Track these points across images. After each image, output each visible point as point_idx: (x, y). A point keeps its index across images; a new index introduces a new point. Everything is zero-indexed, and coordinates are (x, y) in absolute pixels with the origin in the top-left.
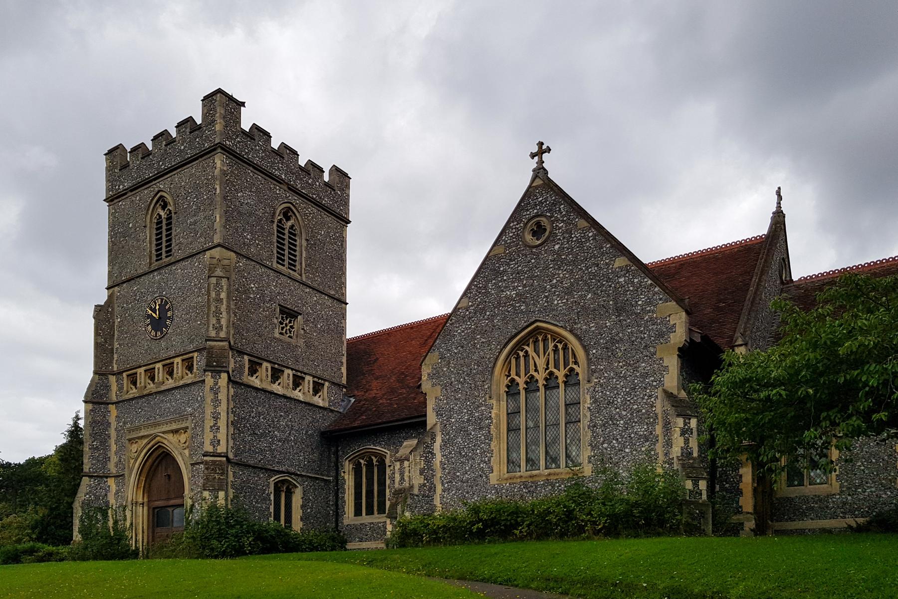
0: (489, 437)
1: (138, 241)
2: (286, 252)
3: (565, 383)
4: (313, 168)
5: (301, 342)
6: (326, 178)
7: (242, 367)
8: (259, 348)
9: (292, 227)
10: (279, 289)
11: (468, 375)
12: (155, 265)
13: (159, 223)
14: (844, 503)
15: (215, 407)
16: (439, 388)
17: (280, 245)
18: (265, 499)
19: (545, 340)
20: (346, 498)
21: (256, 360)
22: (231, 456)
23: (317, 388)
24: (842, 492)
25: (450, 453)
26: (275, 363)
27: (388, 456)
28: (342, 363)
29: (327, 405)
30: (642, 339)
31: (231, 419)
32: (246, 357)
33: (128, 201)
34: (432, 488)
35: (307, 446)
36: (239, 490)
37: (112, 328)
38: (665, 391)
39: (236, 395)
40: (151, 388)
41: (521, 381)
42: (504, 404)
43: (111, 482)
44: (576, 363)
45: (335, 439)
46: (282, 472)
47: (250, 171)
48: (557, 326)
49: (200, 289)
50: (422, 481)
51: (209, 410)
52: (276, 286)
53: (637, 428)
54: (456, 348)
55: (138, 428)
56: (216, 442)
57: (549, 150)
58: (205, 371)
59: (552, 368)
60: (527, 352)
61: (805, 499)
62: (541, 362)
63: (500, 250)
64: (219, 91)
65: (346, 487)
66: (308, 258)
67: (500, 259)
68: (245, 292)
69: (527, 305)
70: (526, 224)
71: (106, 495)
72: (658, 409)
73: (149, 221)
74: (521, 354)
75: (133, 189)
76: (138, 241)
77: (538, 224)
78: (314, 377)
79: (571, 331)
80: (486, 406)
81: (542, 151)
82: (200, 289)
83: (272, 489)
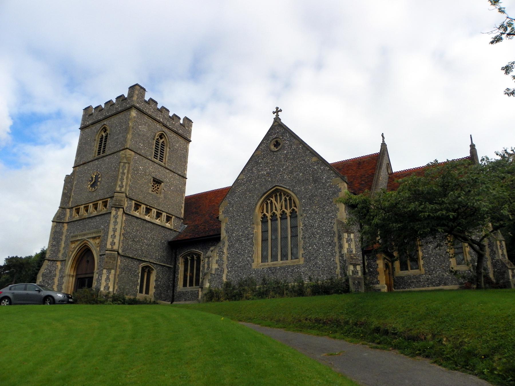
0: (252, 244)
1: (91, 146)
2: (159, 153)
3: (290, 216)
4: (176, 117)
5: (162, 196)
6: (181, 121)
7: (131, 206)
8: (140, 198)
9: (163, 142)
10: (154, 170)
11: (242, 212)
12: (97, 157)
13: (102, 138)
14: (428, 279)
15: (115, 225)
16: (227, 218)
17: (156, 151)
18: (136, 276)
19: (280, 195)
20: (179, 277)
21: (138, 203)
22: (120, 251)
23: (168, 219)
24: (426, 273)
25: (232, 252)
26: (148, 205)
27: (202, 255)
28: (182, 207)
29: (172, 228)
30: (326, 195)
31: (122, 232)
32: (134, 202)
33: (89, 129)
34: (222, 271)
35: (161, 248)
36: (123, 270)
37: (72, 186)
38: (338, 221)
39: (126, 220)
40: (86, 215)
41: (269, 215)
42: (260, 227)
43: (59, 264)
44: (295, 206)
45: (175, 246)
46: (147, 262)
47: (146, 117)
48: (286, 188)
49: (115, 168)
50: (217, 267)
51: (112, 226)
52: (152, 169)
53: (325, 239)
54: (237, 199)
55: (76, 236)
56: (113, 243)
57: (281, 111)
58: (112, 207)
59: (284, 209)
60: (271, 201)
61: (409, 277)
62: (278, 206)
63: (259, 152)
64: (137, 85)
65: (180, 271)
66: (170, 156)
67: (259, 157)
68: (136, 170)
69: (272, 178)
70: (271, 142)
71: (55, 270)
72: (335, 229)
73: (98, 138)
74: (269, 202)
75: (93, 124)
76: (91, 146)
77: (277, 142)
78: (167, 213)
79: (292, 191)
80: (251, 228)
81: (278, 111)
82: (115, 168)
83: (140, 270)
